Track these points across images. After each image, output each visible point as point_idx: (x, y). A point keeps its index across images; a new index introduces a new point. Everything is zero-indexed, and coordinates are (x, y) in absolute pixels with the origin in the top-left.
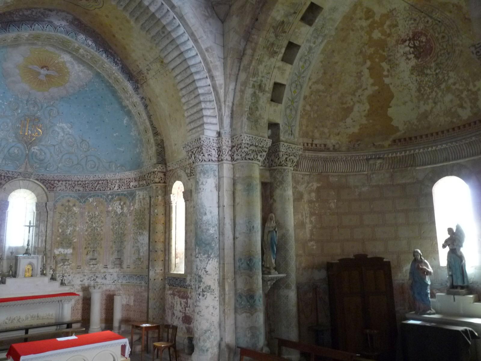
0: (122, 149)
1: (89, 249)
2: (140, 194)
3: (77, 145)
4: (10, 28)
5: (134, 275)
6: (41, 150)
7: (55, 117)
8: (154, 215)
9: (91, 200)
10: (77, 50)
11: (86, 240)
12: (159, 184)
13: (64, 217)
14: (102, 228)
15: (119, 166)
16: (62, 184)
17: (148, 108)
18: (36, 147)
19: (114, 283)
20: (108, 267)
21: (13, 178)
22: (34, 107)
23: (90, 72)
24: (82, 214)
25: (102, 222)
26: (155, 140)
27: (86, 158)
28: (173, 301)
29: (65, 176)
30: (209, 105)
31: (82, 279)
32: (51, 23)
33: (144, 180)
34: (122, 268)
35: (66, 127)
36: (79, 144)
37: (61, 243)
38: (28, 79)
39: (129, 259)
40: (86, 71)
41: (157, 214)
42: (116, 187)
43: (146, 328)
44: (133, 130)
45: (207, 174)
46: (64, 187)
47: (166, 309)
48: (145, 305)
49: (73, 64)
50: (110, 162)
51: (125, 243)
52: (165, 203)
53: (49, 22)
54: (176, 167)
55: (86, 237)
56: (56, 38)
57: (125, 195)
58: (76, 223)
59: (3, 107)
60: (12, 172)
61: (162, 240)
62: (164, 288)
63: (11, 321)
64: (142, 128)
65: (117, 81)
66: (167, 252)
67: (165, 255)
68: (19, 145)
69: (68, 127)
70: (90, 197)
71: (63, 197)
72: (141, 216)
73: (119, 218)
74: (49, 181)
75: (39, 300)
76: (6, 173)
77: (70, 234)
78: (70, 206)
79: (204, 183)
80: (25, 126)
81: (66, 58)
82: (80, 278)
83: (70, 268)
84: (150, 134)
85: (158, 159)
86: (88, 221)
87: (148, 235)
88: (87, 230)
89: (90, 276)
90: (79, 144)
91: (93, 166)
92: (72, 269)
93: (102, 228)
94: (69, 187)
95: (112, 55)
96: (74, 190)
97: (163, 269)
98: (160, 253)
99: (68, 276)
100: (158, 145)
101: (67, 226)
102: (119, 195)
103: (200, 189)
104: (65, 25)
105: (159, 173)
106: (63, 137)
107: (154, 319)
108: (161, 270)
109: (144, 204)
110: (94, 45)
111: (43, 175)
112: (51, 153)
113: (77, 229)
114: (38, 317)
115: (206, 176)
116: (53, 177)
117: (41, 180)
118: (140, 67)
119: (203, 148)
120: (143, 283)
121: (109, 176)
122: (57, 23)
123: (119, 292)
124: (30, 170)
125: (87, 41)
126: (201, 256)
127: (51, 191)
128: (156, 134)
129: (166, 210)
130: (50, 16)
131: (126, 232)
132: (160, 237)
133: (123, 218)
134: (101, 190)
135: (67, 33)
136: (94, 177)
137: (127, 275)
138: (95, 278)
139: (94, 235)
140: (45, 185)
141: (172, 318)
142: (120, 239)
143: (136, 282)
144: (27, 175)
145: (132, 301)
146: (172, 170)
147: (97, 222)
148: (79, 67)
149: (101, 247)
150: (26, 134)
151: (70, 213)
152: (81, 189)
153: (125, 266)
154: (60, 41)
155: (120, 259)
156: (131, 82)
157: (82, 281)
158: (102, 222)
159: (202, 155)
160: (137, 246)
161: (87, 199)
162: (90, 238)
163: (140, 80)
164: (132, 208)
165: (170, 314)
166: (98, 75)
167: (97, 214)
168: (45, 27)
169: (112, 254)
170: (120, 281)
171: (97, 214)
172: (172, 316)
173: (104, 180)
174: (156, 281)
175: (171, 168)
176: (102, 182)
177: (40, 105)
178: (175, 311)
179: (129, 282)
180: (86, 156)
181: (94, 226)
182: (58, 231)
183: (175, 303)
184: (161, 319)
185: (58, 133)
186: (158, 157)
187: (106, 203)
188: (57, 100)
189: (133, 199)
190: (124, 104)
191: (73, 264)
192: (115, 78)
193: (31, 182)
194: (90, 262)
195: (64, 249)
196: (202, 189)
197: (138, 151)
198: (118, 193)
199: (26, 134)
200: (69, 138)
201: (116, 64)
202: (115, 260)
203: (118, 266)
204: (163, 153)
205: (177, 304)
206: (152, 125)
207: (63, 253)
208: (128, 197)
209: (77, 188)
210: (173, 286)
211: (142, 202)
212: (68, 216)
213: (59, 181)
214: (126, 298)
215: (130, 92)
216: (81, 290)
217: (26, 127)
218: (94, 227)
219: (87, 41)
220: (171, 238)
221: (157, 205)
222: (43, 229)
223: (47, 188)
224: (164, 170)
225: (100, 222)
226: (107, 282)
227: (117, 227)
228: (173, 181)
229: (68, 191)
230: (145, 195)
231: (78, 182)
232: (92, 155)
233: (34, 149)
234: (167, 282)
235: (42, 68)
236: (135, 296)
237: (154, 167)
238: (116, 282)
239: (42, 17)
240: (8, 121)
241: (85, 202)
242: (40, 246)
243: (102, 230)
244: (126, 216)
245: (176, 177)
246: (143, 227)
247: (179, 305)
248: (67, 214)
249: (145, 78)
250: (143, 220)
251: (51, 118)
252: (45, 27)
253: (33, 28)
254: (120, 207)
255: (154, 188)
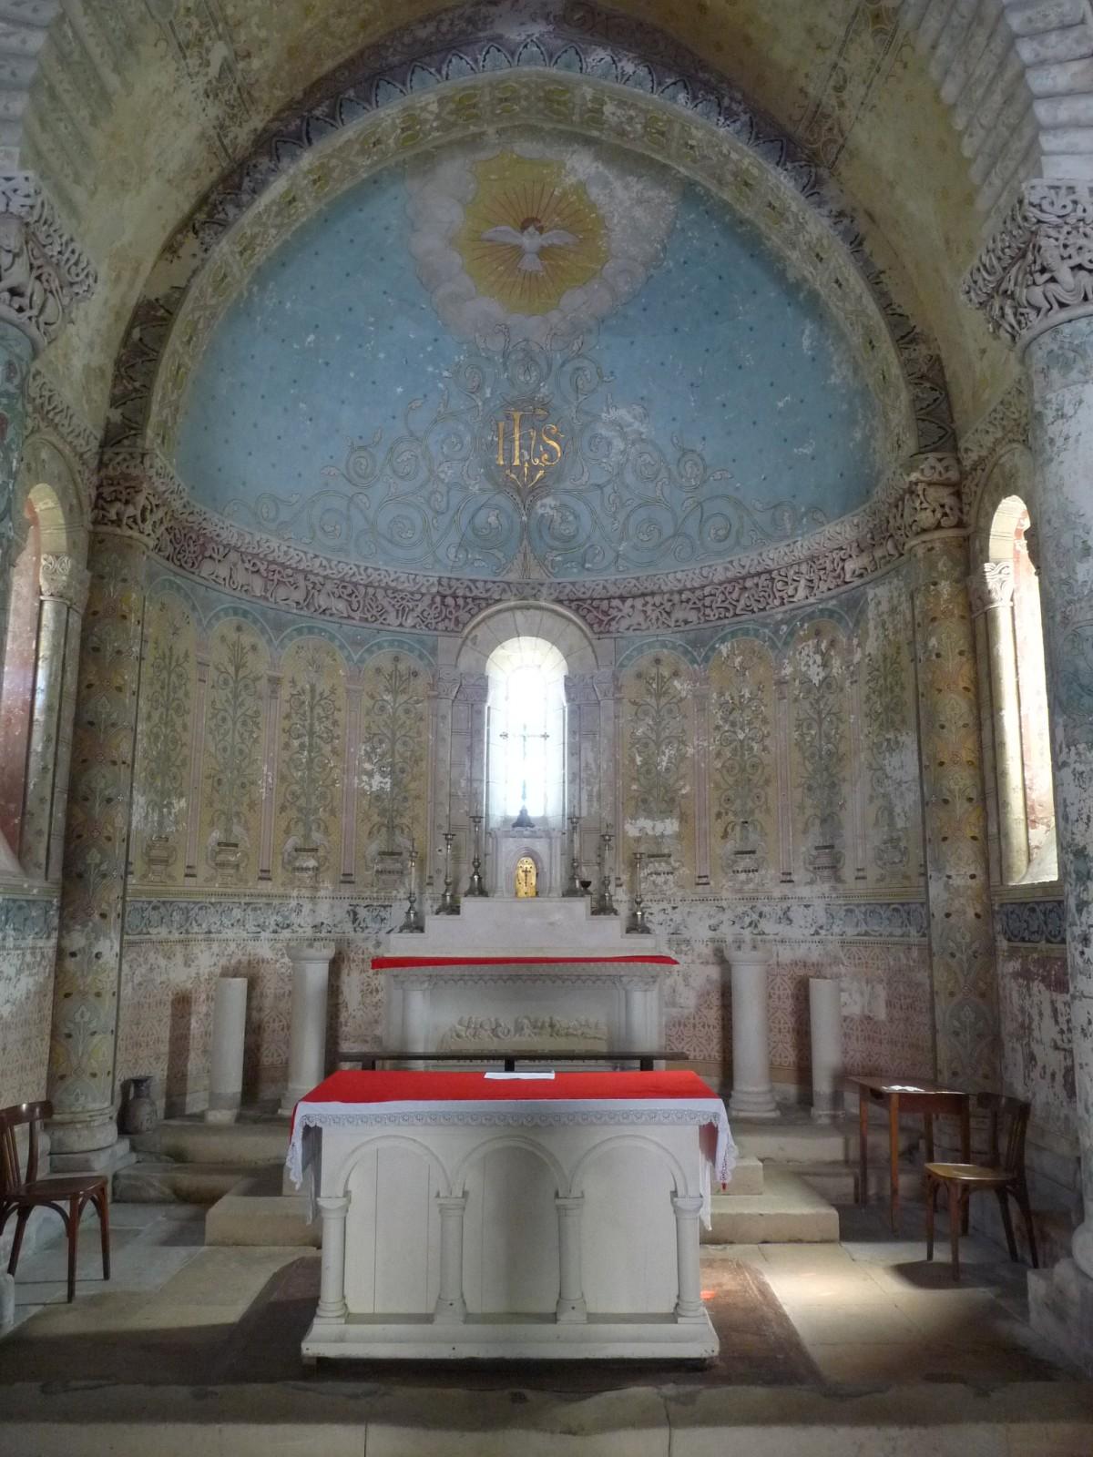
0: (807, 451)
1: (731, 817)
2: (879, 596)
3: (669, 470)
4: (380, 92)
5: (881, 905)
6: (563, 506)
7: (593, 391)
8: (928, 659)
9: (724, 649)
10: (595, 116)
11: (717, 786)
12: (937, 535)
13: (646, 713)
14: (767, 742)
15: (805, 514)
16: (633, 607)
17: (867, 247)
18: (549, 501)
19: (817, 938)
20: (794, 878)
21: (489, 602)
22: (528, 370)
23: (663, 193)
24: (701, 699)
25: (765, 721)
26: (907, 363)
27: (698, 513)
28: (1027, 1003)
29: (638, 579)
30: (1057, 45)
31: (713, 922)
32: (497, 39)
33: (885, 538)
34: (839, 880)
35: (629, 418)
36: (673, 468)
37: (645, 801)
38: (492, 278)
39: (860, 848)
40: (651, 193)
41: (938, 655)
42: (800, 590)
43: (904, 1096)
44: (834, 366)
45: (1080, 365)
46: (641, 619)
47: (1006, 1038)
48: (926, 1019)
49: (607, 184)
50: (775, 507)
51: (846, 789)
52: (969, 607)
53: (491, 39)
54: (988, 441)
55: (718, 777)
56: (524, 92)
57: (831, 613)
58: (683, 731)
59: (441, 385)
60: (485, 582)
61: (966, 754)
62: (991, 951)
63: (471, 1030)
64: (856, 339)
65: (746, 184)
66: (991, 803)
67: (986, 817)
68: (501, 500)
69: (635, 417)
70: (723, 640)
71: (640, 650)
72: (889, 679)
73: (817, 701)
74: (595, 603)
75: (430, 969)
76: (468, 587)
77: (667, 769)
78: (663, 677)
79: (1069, 410)
80: (508, 438)
81: (582, 166)
82: (710, 916)
83: (676, 883)
84: (886, 347)
85: (922, 434)
86: (721, 723)
87: (915, 746)
88: (719, 755)
89: (740, 910)
90: (673, 468)
91: (722, 533)
92: (682, 887)
93: (767, 742)
94: (654, 616)
95: (710, 88)
96: (672, 624)
97: (979, 873)
98: (961, 807)
99: (670, 910)
100: (917, 379)
101: (658, 745)
102: (810, 617)
103: (1052, 441)
104: (542, 35)
105: (931, 491)
106: (623, 452)
107: (955, 1074)
108: (973, 877)
109: (896, 632)
110: (643, 71)
111: (573, 584)
112: (593, 512)
113: (690, 751)
114: (552, 1026)
115: (1074, 375)
116: (604, 587)
117: (572, 601)
118: (811, 90)
119: (1043, 242)
120: (914, 935)
121: (774, 555)
122: (514, 35)
123: (835, 969)
124: (536, 574)
125: (620, 65)
126: (1078, 754)
127: (601, 633)
128: (906, 337)
129: (973, 636)
130: (492, 22)
131: (842, 748)
132: (957, 742)
133: (831, 698)
134: (753, 612)
135: (551, 57)
136: (727, 569)
137: (858, 905)
138: (755, 917)
139: (743, 770)
140: (584, 617)
141: (1027, 1077)
142: (826, 775)
143: (889, 929)
144: (528, 591)
145: (882, 1004)
146: (982, 460)
147: (750, 723)
148: (627, 187)
149: (768, 810)
150: (517, 462)
151: (663, 701)
152: (693, 616)
153: (848, 872)
154: (539, 99)
155: (832, 847)
156: (789, 166)
157: (714, 929)
158: (765, 721)
159: (1041, 279)
160: (884, 795)
161: (713, 649)
162: (731, 780)
163: (825, 144)
164: (857, 657)
165: (1020, 1058)
166: (689, 193)
167: (747, 695)
168: (480, 58)
169: (805, 832)
170: (836, 929)
171: (747, 695)
172: (1026, 1067)
173: (759, 574)
174: (953, 920)
175: (974, 456)
176: (756, 580)
177: (543, 364)
178: (1036, 1048)
179: (866, 934)
180: (700, 504)
181: (741, 736)
182: (633, 760)
183: (1035, 1012)
184: (986, 1077)
185: (610, 444)
186: (922, 425)
187: (772, 654)
188: (590, 331)
189: (857, 623)
190: (791, 275)
191: (685, 871)
192: (735, 175)
193: (546, 615)
194: (735, 862)
195: (653, 819)
196: (1059, 442)
197: (858, 436)
198: (809, 610)
199: (517, 462)
200: (641, 454)
201: (729, 115)
202: (814, 853)
203: (826, 873)
204: (944, 406)
205: (1041, 1015)
206: (887, 306)
207: (650, 833)
208: (841, 619)
209: (679, 614)
210: (1023, 940)
211: (889, 625)
212: (658, 712)
213: (623, 598)
214: (862, 994)
215: (794, 208)
216: (712, 959)
217: (513, 441)
218: (741, 742)
219: (620, 65)
220: (1002, 744)
221: (934, 619)
222: (591, 761)
223: (591, 626)
224: (953, 475)
225: (757, 724)
226: (793, 932)
227: (813, 732)
228: (990, 510)
229: (652, 631)
230: (896, 594)
231: (680, 592)
232: (717, 497)
233: (543, 506)
234: (998, 927)
235: (524, 228)
236: (889, 983)
237: (910, 468)
238: (823, 932)
239: (470, 28)
240: (461, 427)
241: (706, 659)
242: (584, 813)
243: (765, 749)
244: (842, 690)
245: (997, 486)
246: (897, 718)
247: (1048, 1021)
248: (654, 704)
249: (836, 131)
250: (897, 689)
251: (582, 398)
252: (480, 58)
253: (444, 73)
254: (818, 658)
255: (920, 552)
